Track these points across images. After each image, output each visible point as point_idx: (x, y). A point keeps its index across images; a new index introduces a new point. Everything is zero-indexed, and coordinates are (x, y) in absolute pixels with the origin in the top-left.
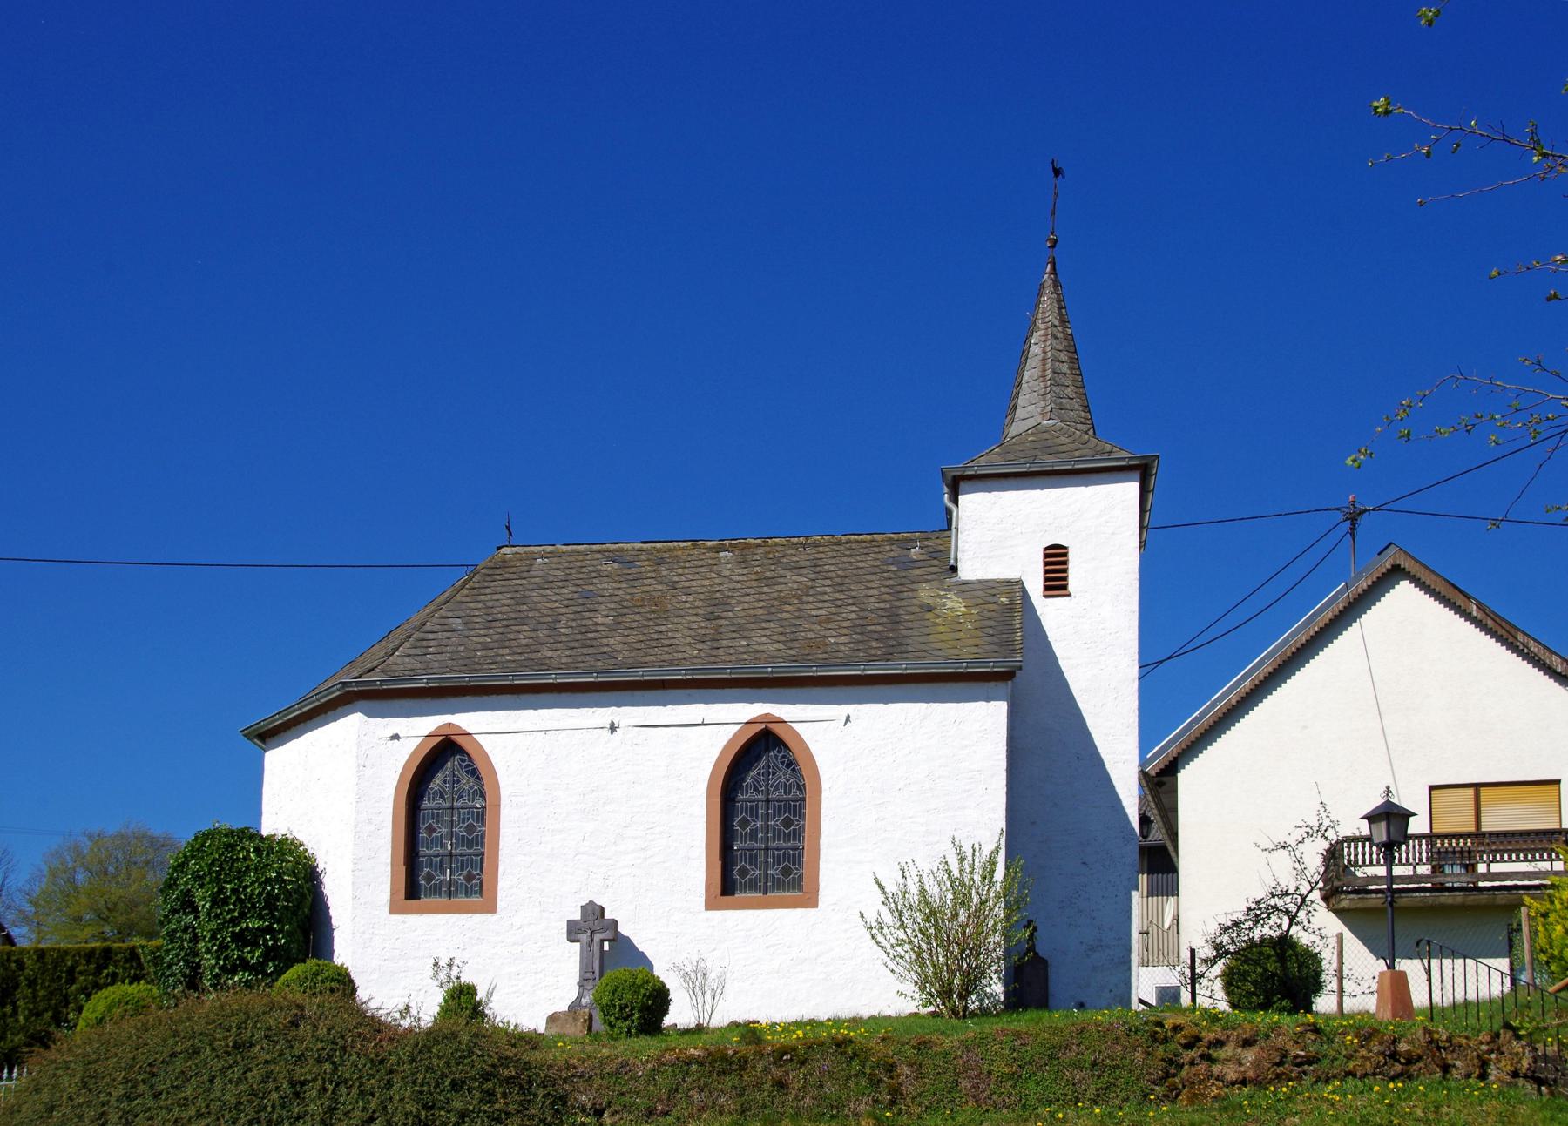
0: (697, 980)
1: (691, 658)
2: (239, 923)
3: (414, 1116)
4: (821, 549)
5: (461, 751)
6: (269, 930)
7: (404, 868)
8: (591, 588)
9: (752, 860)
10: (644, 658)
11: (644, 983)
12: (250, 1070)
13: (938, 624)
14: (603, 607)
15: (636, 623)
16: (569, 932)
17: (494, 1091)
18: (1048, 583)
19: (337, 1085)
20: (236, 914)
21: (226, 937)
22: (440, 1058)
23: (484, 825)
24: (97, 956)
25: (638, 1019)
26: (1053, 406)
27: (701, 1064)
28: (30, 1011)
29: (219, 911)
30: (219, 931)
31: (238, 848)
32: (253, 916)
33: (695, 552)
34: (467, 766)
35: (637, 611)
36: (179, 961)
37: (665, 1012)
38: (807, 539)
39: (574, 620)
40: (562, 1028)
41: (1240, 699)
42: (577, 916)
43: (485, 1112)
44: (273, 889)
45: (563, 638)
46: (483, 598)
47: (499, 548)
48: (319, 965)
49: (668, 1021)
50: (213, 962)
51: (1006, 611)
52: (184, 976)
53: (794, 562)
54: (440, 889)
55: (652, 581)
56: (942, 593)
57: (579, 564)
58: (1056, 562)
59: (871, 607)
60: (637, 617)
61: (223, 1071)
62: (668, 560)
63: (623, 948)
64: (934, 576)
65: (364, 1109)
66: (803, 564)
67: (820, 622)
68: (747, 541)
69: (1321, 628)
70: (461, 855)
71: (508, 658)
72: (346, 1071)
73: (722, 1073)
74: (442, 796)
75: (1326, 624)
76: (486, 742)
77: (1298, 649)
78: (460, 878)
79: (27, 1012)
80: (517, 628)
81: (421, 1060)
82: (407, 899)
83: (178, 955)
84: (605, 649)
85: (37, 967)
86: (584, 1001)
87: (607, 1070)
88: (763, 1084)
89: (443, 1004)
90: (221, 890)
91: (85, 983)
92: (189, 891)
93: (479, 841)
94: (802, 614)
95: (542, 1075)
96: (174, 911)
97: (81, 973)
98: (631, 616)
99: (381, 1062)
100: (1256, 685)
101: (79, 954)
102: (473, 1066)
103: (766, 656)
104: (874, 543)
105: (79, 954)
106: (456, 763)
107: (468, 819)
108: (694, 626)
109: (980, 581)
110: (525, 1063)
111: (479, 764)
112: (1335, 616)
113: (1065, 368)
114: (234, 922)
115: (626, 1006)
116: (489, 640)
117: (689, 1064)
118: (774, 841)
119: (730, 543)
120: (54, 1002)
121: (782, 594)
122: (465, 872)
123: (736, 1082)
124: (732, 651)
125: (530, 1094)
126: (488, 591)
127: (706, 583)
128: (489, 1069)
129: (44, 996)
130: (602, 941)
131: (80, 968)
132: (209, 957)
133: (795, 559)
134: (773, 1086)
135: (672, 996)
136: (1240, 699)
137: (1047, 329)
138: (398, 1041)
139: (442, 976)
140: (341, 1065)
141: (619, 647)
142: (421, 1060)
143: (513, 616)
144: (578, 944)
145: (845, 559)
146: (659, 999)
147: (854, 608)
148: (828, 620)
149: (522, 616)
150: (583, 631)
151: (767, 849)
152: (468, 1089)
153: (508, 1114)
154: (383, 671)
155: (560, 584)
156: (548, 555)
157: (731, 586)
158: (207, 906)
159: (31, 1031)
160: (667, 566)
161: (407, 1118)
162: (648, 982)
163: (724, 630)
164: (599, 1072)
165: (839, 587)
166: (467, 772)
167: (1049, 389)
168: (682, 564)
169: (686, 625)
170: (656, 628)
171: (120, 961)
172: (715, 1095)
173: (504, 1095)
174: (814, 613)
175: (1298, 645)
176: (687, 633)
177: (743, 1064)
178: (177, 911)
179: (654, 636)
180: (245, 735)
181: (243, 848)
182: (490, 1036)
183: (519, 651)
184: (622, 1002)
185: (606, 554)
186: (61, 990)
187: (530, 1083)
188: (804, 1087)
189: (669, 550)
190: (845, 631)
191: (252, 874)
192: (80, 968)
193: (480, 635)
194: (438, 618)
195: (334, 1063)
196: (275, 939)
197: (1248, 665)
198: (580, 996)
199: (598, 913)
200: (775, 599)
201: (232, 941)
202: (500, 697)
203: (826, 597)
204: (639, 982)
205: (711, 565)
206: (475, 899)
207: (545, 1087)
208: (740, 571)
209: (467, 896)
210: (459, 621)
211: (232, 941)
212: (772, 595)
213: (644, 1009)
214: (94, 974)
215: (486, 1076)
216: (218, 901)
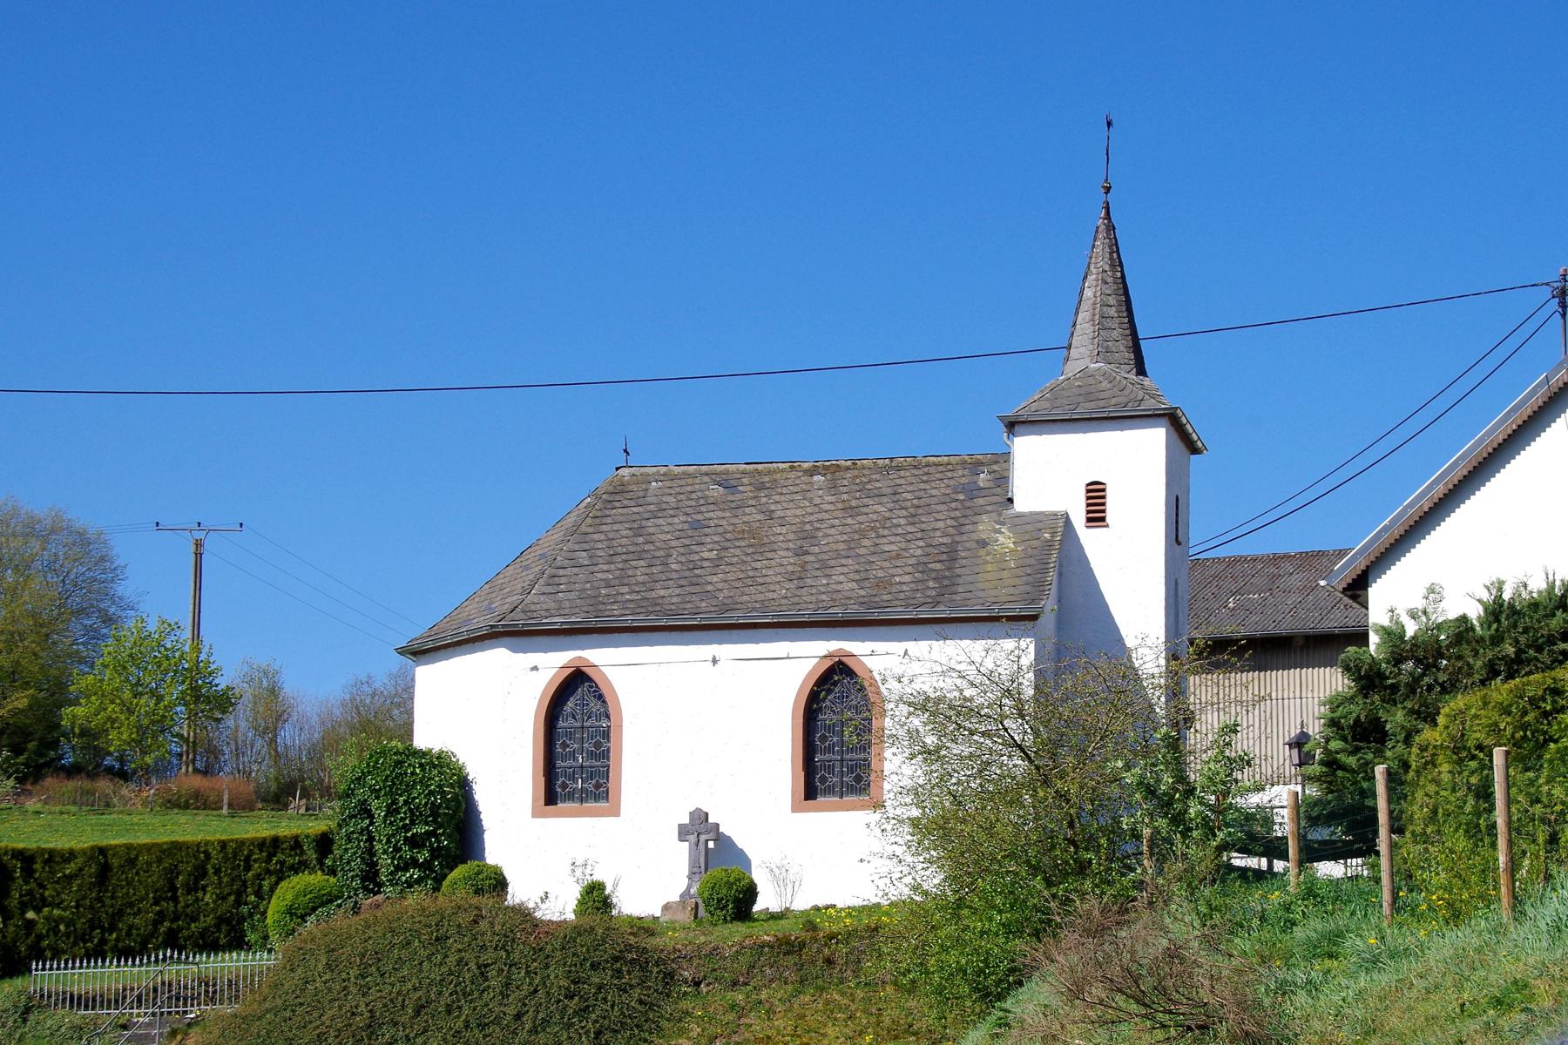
0: (780, 876)
1: (779, 595)
2: (410, 830)
3: (566, 989)
4: (902, 473)
5: (590, 679)
6: (433, 834)
7: (543, 779)
8: (699, 517)
9: (831, 770)
10: (741, 598)
11: (736, 880)
12: (447, 956)
13: (987, 562)
14: (709, 540)
15: (736, 558)
16: (680, 834)
17: (621, 969)
18: (1090, 515)
19: (510, 966)
20: (407, 822)
21: (400, 840)
22: (582, 946)
23: (609, 741)
24: (267, 845)
25: (731, 909)
26: (1100, 349)
27: (772, 947)
28: (217, 895)
29: (393, 819)
30: (393, 835)
31: (406, 765)
32: (420, 822)
33: (792, 475)
34: (595, 691)
35: (737, 544)
36: (357, 858)
37: (754, 902)
38: (892, 461)
39: (683, 554)
40: (673, 915)
41: (1433, 505)
42: (686, 820)
43: (615, 985)
44: (436, 799)
45: (675, 576)
46: (604, 528)
47: (617, 469)
48: (479, 866)
49: (756, 908)
50: (389, 861)
51: (1046, 548)
52: (362, 871)
53: (877, 488)
54: (573, 796)
55: (752, 509)
56: (997, 527)
57: (689, 488)
58: (1096, 495)
59: (936, 542)
60: (738, 552)
61: (429, 958)
62: (768, 485)
63: (724, 842)
64: (995, 507)
65: (530, 984)
66: (885, 491)
67: (891, 558)
68: (838, 463)
69: (1519, 426)
70: (591, 767)
71: (628, 597)
72: (516, 956)
73: (787, 953)
74: (574, 717)
75: (1524, 422)
76: (610, 673)
77: (1494, 449)
78: (590, 786)
79: (214, 896)
80: (635, 562)
81: (569, 948)
82: (546, 805)
83: (355, 853)
84: (709, 588)
85: (220, 856)
86: (692, 891)
87: (703, 953)
88: (816, 961)
89: (580, 897)
90: (394, 802)
91: (259, 870)
92: (366, 800)
93: (605, 755)
94: (877, 549)
95: (656, 957)
96: (352, 817)
97: (255, 861)
98: (732, 551)
99: (541, 950)
100: (1450, 490)
101: (253, 844)
102: (606, 952)
103: (841, 596)
104: (949, 467)
105: (253, 844)
106: (585, 689)
107: (596, 736)
108: (785, 562)
109: (1032, 514)
110: (644, 948)
111: (604, 691)
112: (1535, 412)
113: (1112, 312)
114: (406, 828)
115: (722, 899)
116: (611, 577)
117: (763, 947)
118: (848, 754)
119: (824, 466)
120: (235, 887)
121: (863, 526)
122: (594, 782)
123: (797, 960)
124: (814, 591)
125: (647, 971)
126: (609, 520)
127: (799, 512)
128: (617, 954)
129: (228, 882)
130: (707, 841)
131: (255, 857)
132: (386, 857)
133: (878, 485)
134: (823, 963)
135: (759, 889)
136: (1433, 505)
137: (1098, 274)
138: (552, 934)
139: (578, 873)
140: (511, 952)
141: (720, 586)
142: (569, 948)
143: (632, 549)
144: (687, 843)
145: (922, 486)
146: (751, 892)
147: (921, 543)
148: (898, 556)
149: (639, 549)
150: (691, 567)
151: (842, 760)
152: (603, 969)
153: (632, 987)
154: (524, 612)
155: (671, 512)
156: (662, 478)
157: (820, 516)
158: (383, 814)
159: (219, 913)
160: (766, 492)
161: (560, 990)
162: (739, 880)
163: (809, 568)
164: (697, 954)
165: (912, 519)
166: (595, 696)
167: (1097, 333)
168: (779, 490)
169: (778, 561)
170: (753, 564)
171: (286, 849)
172: (781, 969)
173: (629, 972)
174: (887, 548)
175: (1495, 445)
176: (778, 570)
177: (803, 945)
178: (355, 816)
179: (751, 574)
180: (398, 653)
181: (410, 765)
182: (618, 929)
183: (637, 590)
184: (719, 896)
185: (714, 476)
186: (240, 876)
187: (647, 963)
188: (846, 963)
189: (769, 472)
190: (910, 569)
191: (419, 787)
192: (255, 857)
193: (604, 571)
194: (566, 551)
195: (506, 951)
196: (439, 841)
197: (1425, 483)
198: (689, 887)
199: (703, 818)
200: (857, 532)
201: (405, 844)
202: (621, 634)
203: (900, 531)
204: (732, 879)
205: (805, 491)
206: (602, 804)
207: (658, 966)
208: (830, 499)
209: (596, 801)
210: (584, 554)
211: (405, 844)
212: (854, 527)
213: (737, 901)
214: (265, 862)
215: (616, 959)
216: (392, 810)
